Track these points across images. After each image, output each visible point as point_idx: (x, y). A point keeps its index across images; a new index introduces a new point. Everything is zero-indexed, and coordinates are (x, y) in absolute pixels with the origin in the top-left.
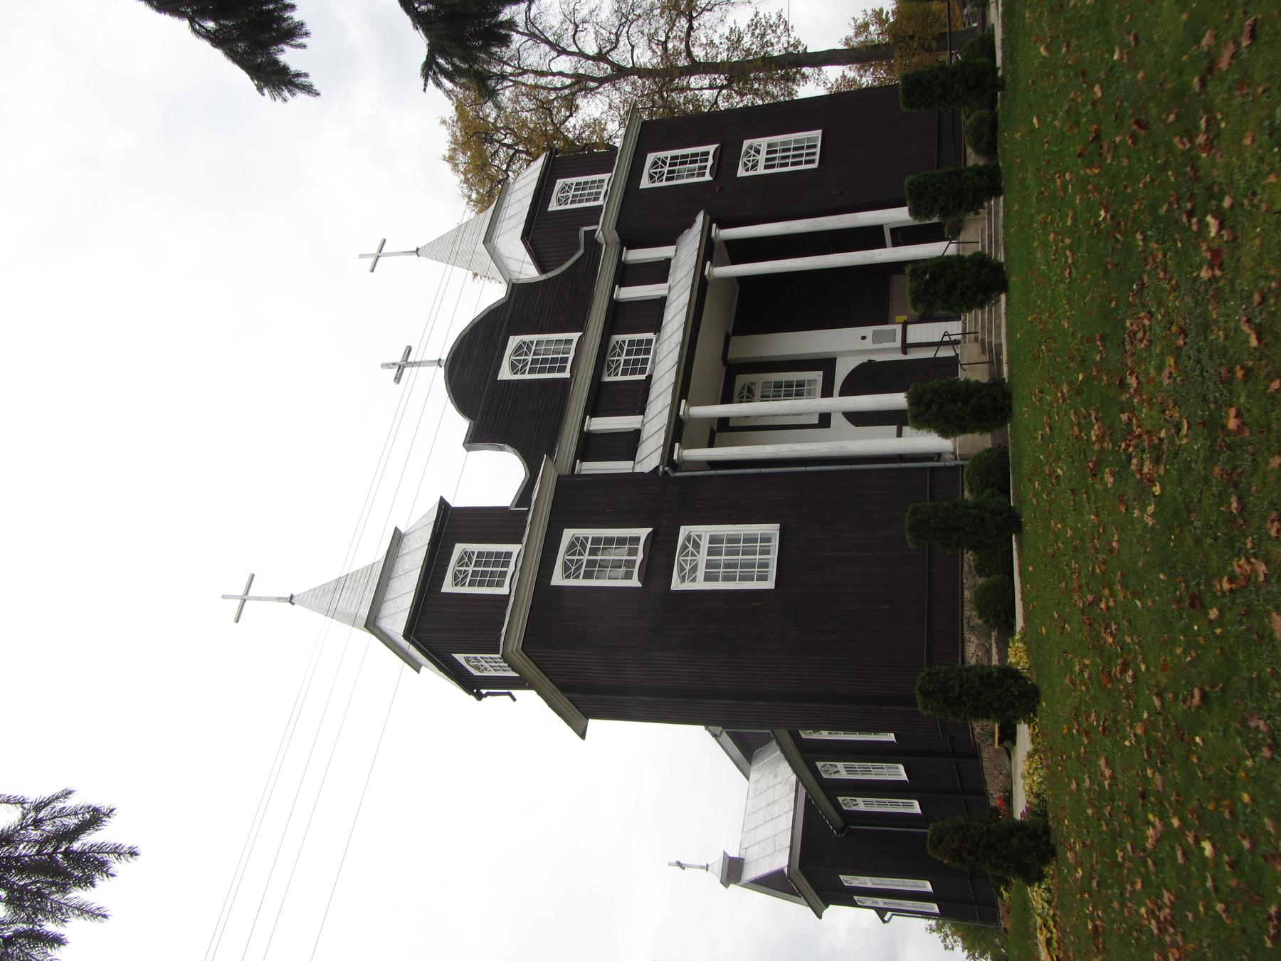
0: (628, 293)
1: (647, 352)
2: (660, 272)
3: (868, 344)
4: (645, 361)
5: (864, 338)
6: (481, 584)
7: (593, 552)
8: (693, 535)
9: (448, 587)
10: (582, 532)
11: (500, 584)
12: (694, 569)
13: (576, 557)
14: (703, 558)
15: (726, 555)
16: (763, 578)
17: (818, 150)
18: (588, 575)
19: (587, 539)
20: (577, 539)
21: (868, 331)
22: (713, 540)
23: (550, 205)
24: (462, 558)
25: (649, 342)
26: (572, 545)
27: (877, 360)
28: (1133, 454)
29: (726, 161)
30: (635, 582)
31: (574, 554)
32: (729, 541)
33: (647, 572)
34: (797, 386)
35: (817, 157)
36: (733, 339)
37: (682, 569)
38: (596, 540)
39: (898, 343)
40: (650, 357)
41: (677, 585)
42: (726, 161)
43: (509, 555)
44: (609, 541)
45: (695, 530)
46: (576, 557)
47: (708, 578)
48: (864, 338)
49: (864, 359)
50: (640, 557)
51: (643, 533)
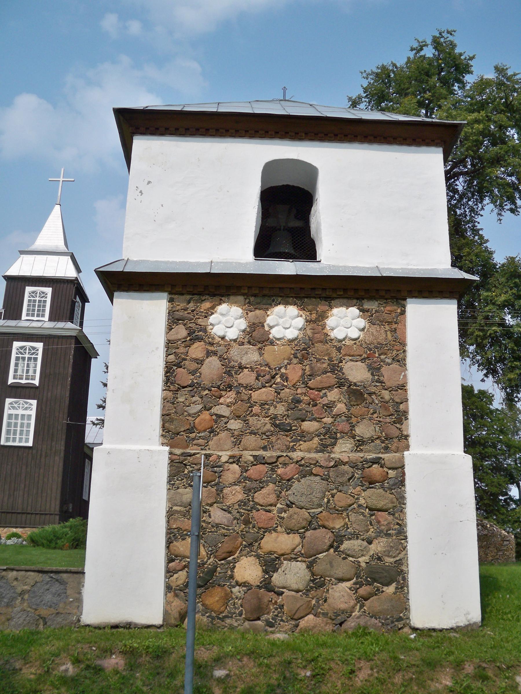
6: (29, 305)
8: (33, 407)
10: (40, 352)
13: (27, 351)
14: (20, 412)
15: (17, 427)
20: (38, 350)
22: (29, 416)
24: (43, 293)
26: (34, 348)
30: (11, 381)
31: (29, 350)
37: (16, 403)
46: (27, 351)
47: (10, 416)
50: (24, 381)
51: (36, 382)
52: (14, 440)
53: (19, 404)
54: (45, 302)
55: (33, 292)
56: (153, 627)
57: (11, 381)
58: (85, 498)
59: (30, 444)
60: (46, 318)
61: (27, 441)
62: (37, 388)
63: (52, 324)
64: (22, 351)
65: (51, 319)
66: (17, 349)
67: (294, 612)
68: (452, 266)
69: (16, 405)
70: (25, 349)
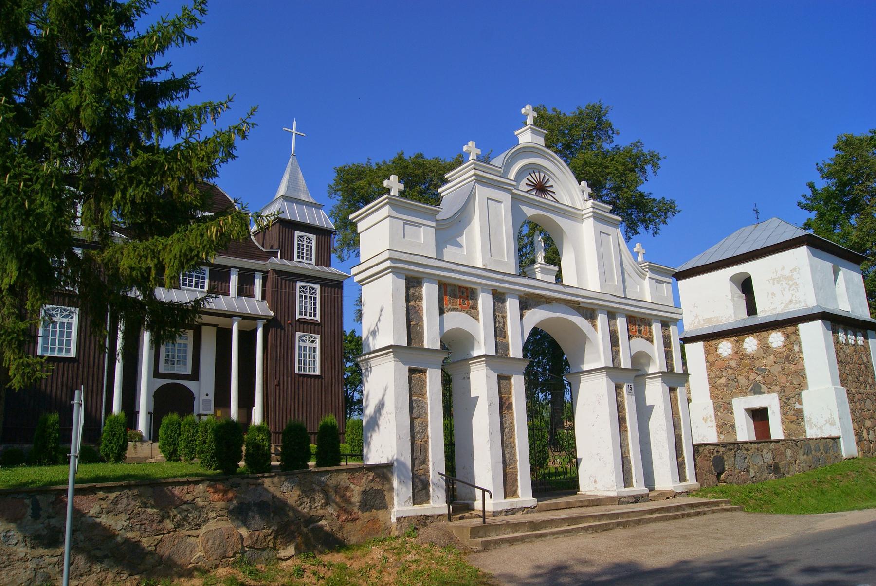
0: (234, 280)
1: (196, 286)
2: (245, 290)
3: (203, 397)
4: (190, 286)
5: (207, 395)
7: (310, 297)
9: (297, 234)
10: (318, 292)
11: (299, 257)
12: (303, 341)
14: (308, 344)
16: (300, 369)
17: (307, 373)
18: (301, 296)
19: (205, 274)
21: (212, 397)
22: (315, 349)
23: (299, 232)
25: (203, 287)
26: (313, 289)
27: (195, 402)
28: (214, 515)
29: (308, 326)
30: (298, 316)
31: (310, 290)
32: (314, 355)
33: (302, 322)
34: (168, 357)
35: (302, 372)
36: (215, 329)
37: (304, 336)
38: (315, 299)
39: (201, 412)
40: (193, 288)
41: (298, 334)
42: (308, 326)
43: (311, 259)
44: (315, 304)
45: (318, 341)
48: (207, 395)
49: (196, 395)
50: (308, 317)
51: (318, 318)
52: (53, 350)
53: (58, 311)
54: (311, 247)
55: (301, 237)
56: (586, 504)
57: (298, 316)
58: (137, 410)
59: (72, 354)
60: (313, 261)
61: (68, 351)
62: (319, 325)
63: (318, 268)
64: (304, 290)
65: (317, 264)
66: (300, 288)
67: (465, 480)
68: (748, 315)
69: (304, 338)
70: (306, 289)
